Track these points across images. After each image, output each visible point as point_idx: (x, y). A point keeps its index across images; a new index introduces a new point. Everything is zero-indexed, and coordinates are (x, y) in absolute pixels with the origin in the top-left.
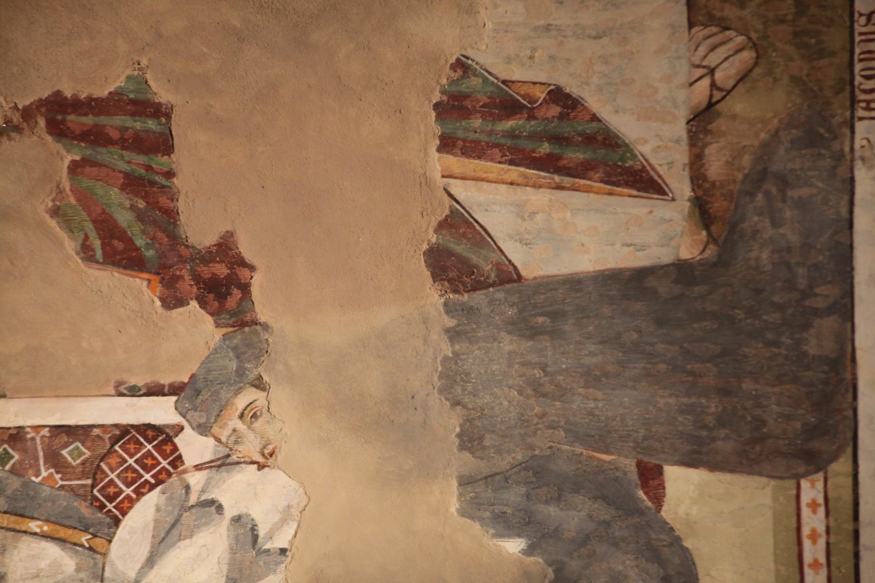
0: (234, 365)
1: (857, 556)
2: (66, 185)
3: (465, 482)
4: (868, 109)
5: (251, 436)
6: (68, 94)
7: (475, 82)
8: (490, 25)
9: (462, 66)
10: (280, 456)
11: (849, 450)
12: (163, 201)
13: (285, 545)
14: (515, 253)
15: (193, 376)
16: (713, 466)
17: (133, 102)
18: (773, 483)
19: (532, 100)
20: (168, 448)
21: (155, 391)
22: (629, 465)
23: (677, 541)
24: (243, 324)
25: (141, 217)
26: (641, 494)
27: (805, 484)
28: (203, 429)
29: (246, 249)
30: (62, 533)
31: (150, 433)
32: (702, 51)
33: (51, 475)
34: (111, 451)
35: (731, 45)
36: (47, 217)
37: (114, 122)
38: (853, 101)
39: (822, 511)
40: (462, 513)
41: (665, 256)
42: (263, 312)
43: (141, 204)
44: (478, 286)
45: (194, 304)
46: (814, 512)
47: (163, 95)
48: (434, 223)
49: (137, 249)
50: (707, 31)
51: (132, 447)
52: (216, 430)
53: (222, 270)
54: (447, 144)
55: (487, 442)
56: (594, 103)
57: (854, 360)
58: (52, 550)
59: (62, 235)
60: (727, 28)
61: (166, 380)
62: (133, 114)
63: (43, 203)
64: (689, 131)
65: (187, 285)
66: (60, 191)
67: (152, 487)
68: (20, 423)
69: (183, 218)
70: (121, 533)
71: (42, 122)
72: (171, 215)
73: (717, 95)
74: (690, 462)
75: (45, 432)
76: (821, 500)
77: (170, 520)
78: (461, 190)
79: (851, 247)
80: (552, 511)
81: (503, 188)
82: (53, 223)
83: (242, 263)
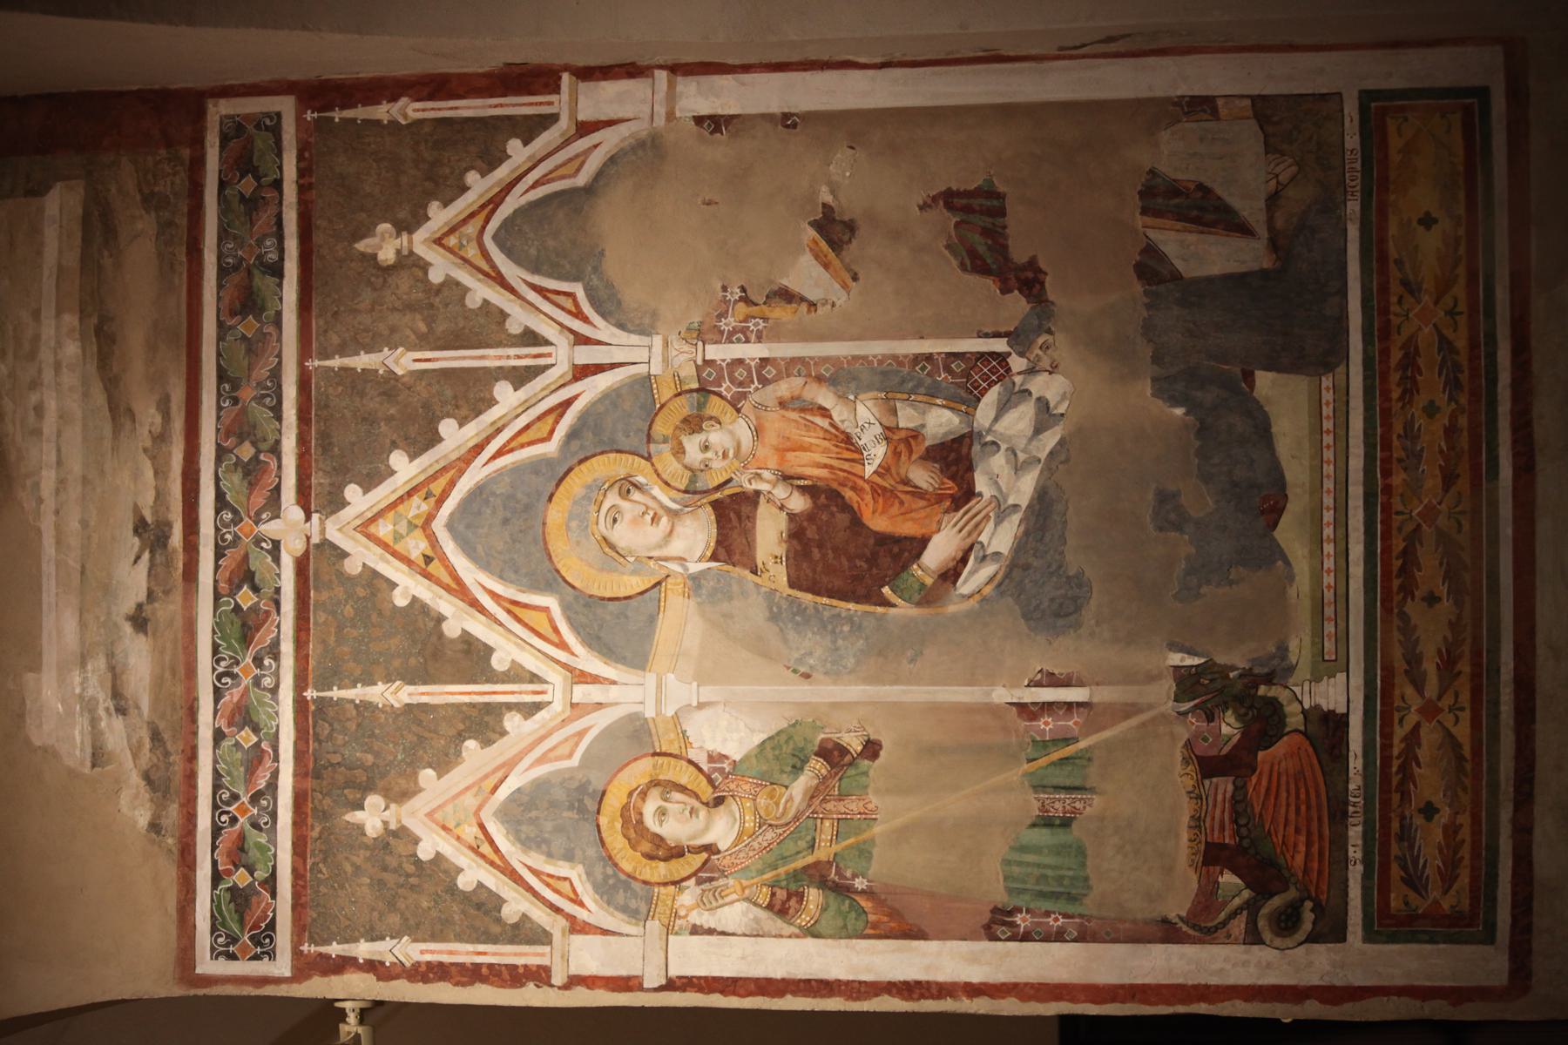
0: (1036, 322)
1: (1348, 412)
2: (953, 233)
3: (1154, 380)
4: (1352, 195)
5: (1045, 357)
6: (955, 189)
7: (1159, 180)
8: (1166, 152)
9: (1152, 172)
10: (1060, 368)
11: (1345, 362)
12: (1001, 240)
13: (1063, 411)
14: (1180, 265)
15: (1016, 328)
16: (1279, 371)
17: (986, 192)
18: (1308, 378)
19: (1188, 189)
20: (1004, 364)
21: (997, 335)
22: (1237, 370)
23: (1261, 407)
24: (1041, 302)
25: (990, 248)
26: (1243, 385)
27: (1323, 379)
28: (1021, 354)
29: (1042, 265)
30: (952, 405)
31: (995, 356)
32: (1272, 165)
33: (946, 377)
34: (976, 365)
35: (1286, 164)
36: (943, 249)
37: (976, 203)
38: (1346, 192)
39: (1331, 391)
40: (1153, 395)
41: (1255, 266)
42: (1051, 296)
43: (990, 242)
44: (1161, 281)
45: (1016, 292)
46: (1328, 392)
47: (1001, 188)
48: (1138, 250)
49: (988, 265)
50: (1274, 157)
51: (986, 363)
52: (1027, 355)
53: (1030, 275)
54: (1144, 212)
55: (1166, 360)
56: (1219, 191)
57: (1347, 317)
58: (947, 413)
59: (952, 258)
60: (1284, 155)
61: (1003, 330)
62: (986, 198)
63: (942, 243)
64: (1267, 205)
65: (1013, 282)
66: (950, 237)
67: (996, 383)
68: (931, 351)
69: (1011, 249)
70: (981, 405)
71: (941, 203)
72: (1005, 247)
73: (1280, 187)
74: (1268, 369)
75: (943, 355)
76: (1331, 386)
77: (1005, 399)
78: (1152, 234)
79: (1346, 262)
80: (1199, 394)
81: (1173, 233)
82: (946, 252)
83: (1041, 271)
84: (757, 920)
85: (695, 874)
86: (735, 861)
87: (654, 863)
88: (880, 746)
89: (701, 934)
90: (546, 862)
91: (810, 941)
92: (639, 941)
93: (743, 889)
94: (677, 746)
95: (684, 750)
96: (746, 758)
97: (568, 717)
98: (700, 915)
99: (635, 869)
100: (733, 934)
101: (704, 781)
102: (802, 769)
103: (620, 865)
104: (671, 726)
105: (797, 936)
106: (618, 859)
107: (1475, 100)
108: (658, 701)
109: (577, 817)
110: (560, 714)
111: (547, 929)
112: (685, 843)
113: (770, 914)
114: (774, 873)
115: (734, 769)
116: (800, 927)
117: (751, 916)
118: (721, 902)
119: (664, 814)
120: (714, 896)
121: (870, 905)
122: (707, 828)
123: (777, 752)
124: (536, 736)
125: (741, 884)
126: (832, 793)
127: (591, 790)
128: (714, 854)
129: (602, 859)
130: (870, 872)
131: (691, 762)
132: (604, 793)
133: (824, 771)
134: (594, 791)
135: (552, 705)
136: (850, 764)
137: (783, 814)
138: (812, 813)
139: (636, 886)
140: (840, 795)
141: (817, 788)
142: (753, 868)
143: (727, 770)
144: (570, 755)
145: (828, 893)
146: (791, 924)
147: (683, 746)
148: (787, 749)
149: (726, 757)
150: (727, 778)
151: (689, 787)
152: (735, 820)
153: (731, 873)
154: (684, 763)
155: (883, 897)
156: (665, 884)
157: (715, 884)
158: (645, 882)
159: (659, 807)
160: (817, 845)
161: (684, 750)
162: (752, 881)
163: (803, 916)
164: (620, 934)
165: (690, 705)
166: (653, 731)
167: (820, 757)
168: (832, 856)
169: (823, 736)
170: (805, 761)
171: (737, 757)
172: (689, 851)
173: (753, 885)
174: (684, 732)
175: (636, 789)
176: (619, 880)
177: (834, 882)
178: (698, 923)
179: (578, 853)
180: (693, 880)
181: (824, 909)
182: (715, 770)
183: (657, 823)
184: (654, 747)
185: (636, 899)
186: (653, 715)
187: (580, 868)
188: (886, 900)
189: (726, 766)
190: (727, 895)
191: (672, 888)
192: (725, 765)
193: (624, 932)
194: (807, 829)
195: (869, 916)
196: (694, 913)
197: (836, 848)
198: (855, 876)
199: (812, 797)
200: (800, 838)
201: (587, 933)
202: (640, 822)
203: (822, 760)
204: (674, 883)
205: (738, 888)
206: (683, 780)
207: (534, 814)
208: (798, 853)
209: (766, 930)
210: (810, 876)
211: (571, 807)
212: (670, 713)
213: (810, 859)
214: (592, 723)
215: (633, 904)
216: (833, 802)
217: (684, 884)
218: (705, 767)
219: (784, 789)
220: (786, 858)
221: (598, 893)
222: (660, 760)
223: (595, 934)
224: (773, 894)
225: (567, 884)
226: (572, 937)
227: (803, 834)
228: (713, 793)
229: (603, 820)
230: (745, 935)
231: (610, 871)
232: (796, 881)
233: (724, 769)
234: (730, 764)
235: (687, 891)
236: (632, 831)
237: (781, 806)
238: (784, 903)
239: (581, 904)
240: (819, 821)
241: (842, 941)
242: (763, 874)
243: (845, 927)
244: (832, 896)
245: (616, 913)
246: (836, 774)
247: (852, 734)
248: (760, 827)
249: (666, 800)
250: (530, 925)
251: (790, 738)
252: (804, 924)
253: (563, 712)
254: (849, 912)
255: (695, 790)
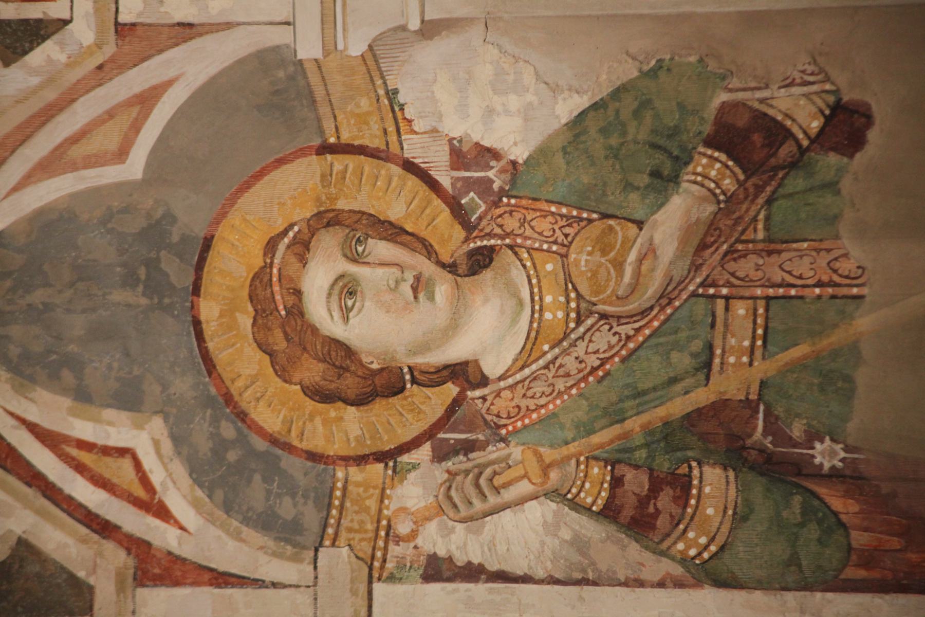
84: (579, 544)
85: (429, 434)
86: (524, 403)
87: (332, 411)
88: (868, 118)
89: (449, 580)
90: (72, 412)
91: (708, 596)
92: (303, 598)
93: (545, 469)
94: (376, 128)
95: (393, 138)
96: (541, 155)
97: (112, 60)
98: (447, 532)
99: (288, 424)
100: (526, 579)
101: (445, 214)
102: (674, 179)
103: (253, 415)
104: (360, 79)
105: (679, 584)
106: (246, 400)
107: (472, 194)
108: (328, 20)
109: (144, 301)
110: (90, 51)
111: (81, 574)
112: (405, 361)
113: (612, 528)
114: (617, 430)
115: (513, 182)
116: (684, 561)
117: (566, 535)
118: (493, 500)
119: (352, 293)
120: (477, 486)
121: (854, 507)
122: (453, 327)
123: (614, 141)
124: (35, 105)
125: (539, 457)
126: (749, 235)
127: (175, 238)
128: (475, 387)
129: (209, 402)
130: (851, 426)
131: (410, 167)
132: (207, 244)
133: (728, 183)
134: (184, 239)
135: (70, 26)
136: (793, 165)
137: (634, 288)
138: (702, 285)
139: (293, 465)
140: (769, 240)
141: (712, 225)
142: (566, 419)
143: (496, 186)
144: (121, 154)
145: (751, 476)
146: (663, 554)
147: (391, 129)
148: (639, 132)
149: (495, 154)
150: (497, 204)
151: (409, 228)
152: (521, 303)
153: (516, 431)
154: (396, 170)
155: (886, 488)
156: (361, 460)
157: (478, 457)
158: (313, 457)
159: (342, 276)
160: (717, 361)
161: (393, 138)
162: (565, 451)
163: (691, 535)
164: (258, 583)
165: (403, 28)
166: (319, 92)
167: (718, 148)
168: (755, 388)
169: (724, 97)
170: (683, 160)
171: (520, 154)
172: (414, 381)
173: (568, 458)
174: (392, 95)
175: (285, 233)
176: (252, 452)
177: (762, 451)
178: (442, 552)
179: (153, 389)
180: (425, 451)
181: (741, 518)
182: (470, 185)
183: (336, 314)
184: (321, 131)
185: (293, 495)
186: (318, 54)
187: (157, 425)
188: (699, 440)
189: (494, 175)
190: (506, 485)
191: (377, 469)
192: (491, 174)
193: (268, 579)
194: (693, 324)
195: (854, 534)
196: (432, 527)
197: (763, 368)
198: (813, 437)
199: (703, 246)
200: (676, 346)
201: (177, 583)
202: (297, 311)
203: (723, 157)
204: (382, 457)
205: (534, 468)
206: (395, 212)
207: (38, 296)
208: (673, 381)
209: (603, 567)
210: (704, 437)
211: (130, 281)
212: (357, 48)
213: (702, 397)
214: (171, 73)
215: (286, 509)
216: (753, 258)
217: (405, 458)
218: (445, 180)
219: (633, 229)
220: (644, 393)
221: (201, 486)
222: (338, 162)
223: (196, 584)
224: (617, 482)
225: (126, 464)
226: (143, 593)
227: (682, 335)
228: (467, 240)
229: (209, 310)
230: (553, 581)
231: (228, 431)
232: (671, 449)
233: (491, 182)
234: (502, 171)
235: (412, 476)
236: (278, 334)
237: (628, 271)
238: (643, 502)
239: (162, 513)
240: (720, 303)
241: (790, 596)
242: (590, 432)
243: (793, 561)
244: (758, 485)
245: (247, 532)
246: (759, 189)
247: (797, 90)
248: (579, 322)
249: (355, 259)
250: (37, 568)
251: (646, 104)
252: (693, 552)
253: (99, 45)
254: (802, 525)
255: (423, 234)
